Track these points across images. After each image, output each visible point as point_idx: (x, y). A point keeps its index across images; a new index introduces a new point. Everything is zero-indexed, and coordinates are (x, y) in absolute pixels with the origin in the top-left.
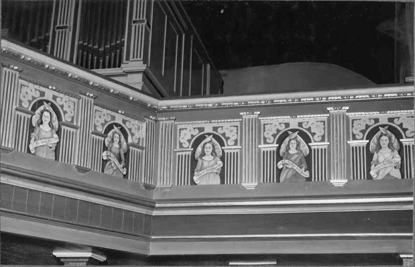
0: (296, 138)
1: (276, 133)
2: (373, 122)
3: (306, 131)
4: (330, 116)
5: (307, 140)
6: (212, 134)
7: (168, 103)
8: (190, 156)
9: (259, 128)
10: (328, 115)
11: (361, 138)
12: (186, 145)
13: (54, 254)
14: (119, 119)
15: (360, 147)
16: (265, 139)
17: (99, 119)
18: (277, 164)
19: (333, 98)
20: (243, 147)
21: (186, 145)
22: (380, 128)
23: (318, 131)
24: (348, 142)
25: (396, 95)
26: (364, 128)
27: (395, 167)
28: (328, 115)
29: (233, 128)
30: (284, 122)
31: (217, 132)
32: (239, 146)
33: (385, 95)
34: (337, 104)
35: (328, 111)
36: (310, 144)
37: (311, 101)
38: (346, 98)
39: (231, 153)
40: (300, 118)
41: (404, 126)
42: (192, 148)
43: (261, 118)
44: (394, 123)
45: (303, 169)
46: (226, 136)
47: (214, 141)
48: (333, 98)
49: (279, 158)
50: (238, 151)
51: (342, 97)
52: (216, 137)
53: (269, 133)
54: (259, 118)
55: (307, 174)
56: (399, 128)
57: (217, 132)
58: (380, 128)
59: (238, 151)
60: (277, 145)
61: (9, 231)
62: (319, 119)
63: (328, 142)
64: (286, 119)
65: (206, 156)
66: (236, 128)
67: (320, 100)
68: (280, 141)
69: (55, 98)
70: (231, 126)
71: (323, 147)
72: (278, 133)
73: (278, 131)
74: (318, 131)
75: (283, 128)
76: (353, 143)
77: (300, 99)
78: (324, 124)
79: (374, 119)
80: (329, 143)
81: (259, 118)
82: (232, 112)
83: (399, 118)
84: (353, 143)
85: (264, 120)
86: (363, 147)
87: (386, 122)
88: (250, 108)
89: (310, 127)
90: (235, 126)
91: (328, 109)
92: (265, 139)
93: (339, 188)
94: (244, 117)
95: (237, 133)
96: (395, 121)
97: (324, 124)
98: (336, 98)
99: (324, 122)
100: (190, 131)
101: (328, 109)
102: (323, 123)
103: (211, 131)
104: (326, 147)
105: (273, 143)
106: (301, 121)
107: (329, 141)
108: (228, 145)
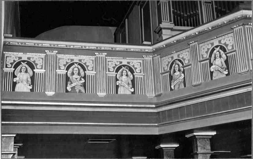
0: (218, 51)
1: (135, 67)
2: (70, 61)
3: (83, 64)
4: (96, 57)
5: (32, 68)
6: (78, 63)
7: (158, 45)
8: (65, 75)
9: (57, 60)
10: (45, 55)
11: (113, 71)
12: (112, 70)
13: (186, 136)
14: (175, 57)
15: (38, 73)
16: (6, 65)
17: (185, 55)
18: (116, 82)
19: (45, 45)
20: (55, 71)
21: (112, 70)
22: (21, 62)
23: (40, 63)
24: (56, 71)
25: (96, 48)
26: (13, 62)
27: (81, 86)
28: (45, 55)
29: (138, 63)
30: (18, 56)
31: (30, 60)
32: (142, 73)
33: (43, 45)
34: (51, 49)
35: (95, 55)
36: (85, 72)
37: (33, 45)
38: (68, 46)
39: (110, 76)
40: (29, 55)
41: (65, 63)
42: (14, 68)
43: (58, 55)
44: (30, 60)
45: (130, 88)
46: (36, 62)
47: (79, 67)
48: (45, 45)
49: (117, 80)
50: (142, 76)
51: (18, 43)
52: (80, 64)
53: (62, 63)
54: (106, 57)
55: (132, 90)
56: (84, 65)
57: (30, 60)
58: (21, 62)
59: (142, 76)
60: (14, 69)
61: (217, 124)
62: (91, 59)
63: (44, 69)
64: (20, 54)
65: (75, 75)
66: (140, 63)
67: (69, 47)
68: (67, 69)
69: (220, 42)
70: (137, 62)
71: (93, 75)
72: (67, 64)
73: (67, 63)
74: (40, 63)
75: (17, 60)
76: (59, 71)
77: (10, 43)
78: (43, 60)
79: (119, 62)
80: (96, 73)
81: (106, 57)
82: (41, 50)
83: (33, 58)
84: (59, 71)
85: (59, 56)
86: (42, 74)
87: (78, 61)
88: (100, 51)
89: (86, 63)
90: (139, 62)
91: (46, 51)
92: (109, 69)
93: (50, 97)
94: (97, 55)
95: (43, 62)
96: (82, 61)
97: (43, 60)
98: (63, 46)
99: (93, 60)
100: (13, 58)
101: (46, 51)
102: (140, 63)
103: (126, 64)
104: (94, 75)
105: (113, 71)
106: (81, 59)
107: (95, 71)
108: (136, 72)
